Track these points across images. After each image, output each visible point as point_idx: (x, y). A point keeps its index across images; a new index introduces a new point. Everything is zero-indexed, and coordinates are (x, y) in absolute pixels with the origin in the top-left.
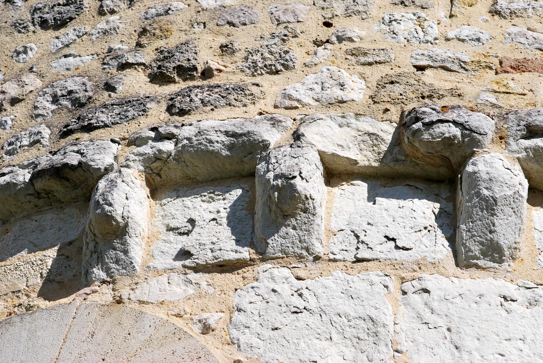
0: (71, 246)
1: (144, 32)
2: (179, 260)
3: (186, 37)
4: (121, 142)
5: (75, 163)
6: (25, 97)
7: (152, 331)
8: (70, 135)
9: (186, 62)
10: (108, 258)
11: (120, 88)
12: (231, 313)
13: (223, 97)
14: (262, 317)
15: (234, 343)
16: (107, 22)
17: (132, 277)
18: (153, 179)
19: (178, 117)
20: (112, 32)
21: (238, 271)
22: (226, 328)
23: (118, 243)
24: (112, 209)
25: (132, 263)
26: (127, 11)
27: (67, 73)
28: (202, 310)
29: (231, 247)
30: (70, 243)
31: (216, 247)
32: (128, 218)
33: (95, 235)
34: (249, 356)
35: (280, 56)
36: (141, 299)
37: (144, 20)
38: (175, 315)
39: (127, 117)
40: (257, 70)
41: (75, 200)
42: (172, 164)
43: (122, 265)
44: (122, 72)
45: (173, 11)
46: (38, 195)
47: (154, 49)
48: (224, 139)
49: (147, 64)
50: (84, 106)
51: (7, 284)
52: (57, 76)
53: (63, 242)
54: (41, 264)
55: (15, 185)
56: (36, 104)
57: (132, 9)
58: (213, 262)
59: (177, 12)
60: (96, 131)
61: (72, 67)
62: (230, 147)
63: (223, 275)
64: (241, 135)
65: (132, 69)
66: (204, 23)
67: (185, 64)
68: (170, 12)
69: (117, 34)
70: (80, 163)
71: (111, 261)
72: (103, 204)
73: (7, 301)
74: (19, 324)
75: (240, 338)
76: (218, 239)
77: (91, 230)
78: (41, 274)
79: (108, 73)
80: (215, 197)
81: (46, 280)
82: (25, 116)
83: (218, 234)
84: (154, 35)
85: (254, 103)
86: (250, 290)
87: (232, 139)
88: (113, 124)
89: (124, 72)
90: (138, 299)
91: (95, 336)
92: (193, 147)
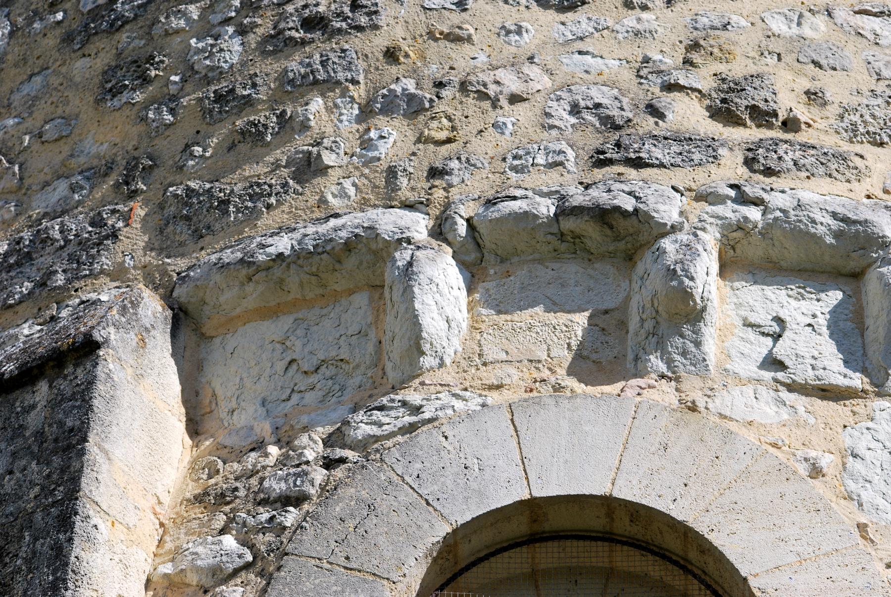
0: (608, 316)
1: (695, 46)
2: (766, 370)
3: (755, 67)
4: (685, 193)
5: (630, 208)
6: (530, 97)
7: (748, 460)
8: (608, 165)
9: (763, 103)
10: (672, 346)
11: (670, 116)
12: (843, 457)
13: (822, 164)
14: (885, 471)
15: (853, 499)
16: (639, 20)
17: (704, 378)
18: (726, 252)
19: (762, 176)
20: (647, 35)
21: (845, 402)
22: (838, 476)
23: (688, 329)
24: (694, 284)
25: (704, 360)
26: (665, 11)
27: (585, 76)
28: (803, 444)
29: (838, 368)
30: (606, 312)
31: (819, 364)
32: (708, 300)
33: (657, 312)
34: (874, 520)
35: (885, 124)
36: (723, 412)
37: (692, 30)
38: (770, 444)
39: (693, 160)
40: (857, 136)
41: (612, 255)
42: (756, 238)
43: (691, 359)
44: (668, 95)
45: (733, 27)
46: (562, 236)
47: (712, 73)
48: (830, 222)
49: (704, 91)
50: (620, 129)
51: (519, 347)
52: (573, 77)
53: (597, 309)
54: (566, 331)
55: (536, 217)
56: (547, 110)
57: (672, 11)
58: (815, 383)
59: (738, 29)
60: (648, 169)
61: (592, 70)
62: (838, 235)
63: (825, 402)
64: (855, 222)
65: (682, 93)
66: (779, 55)
67: (762, 105)
68: (729, 27)
69: (654, 39)
70: (636, 210)
71: (676, 351)
72: (681, 275)
73: (522, 371)
74: (554, 409)
75: (862, 494)
76: (820, 354)
77: (653, 305)
78: (569, 345)
79: (648, 91)
80: (806, 294)
81: (576, 354)
82: (533, 123)
83: (819, 347)
84: (711, 54)
85: (859, 181)
86: (865, 431)
87: (842, 224)
88: (672, 165)
89: (672, 95)
90: (719, 411)
91: (668, 450)
92: (789, 223)
